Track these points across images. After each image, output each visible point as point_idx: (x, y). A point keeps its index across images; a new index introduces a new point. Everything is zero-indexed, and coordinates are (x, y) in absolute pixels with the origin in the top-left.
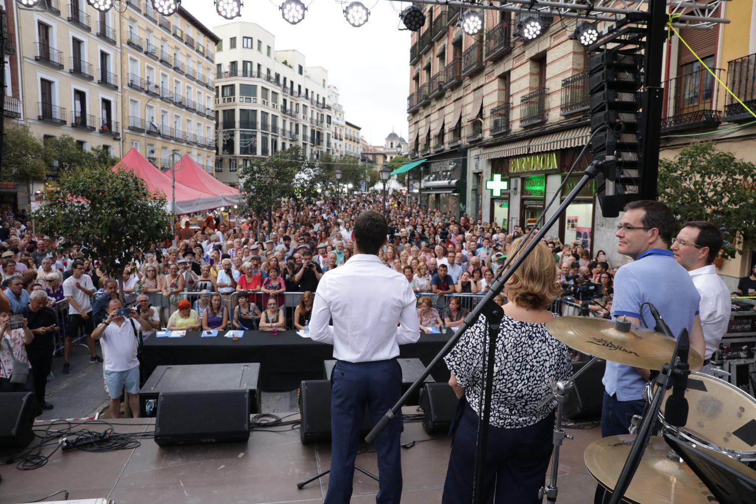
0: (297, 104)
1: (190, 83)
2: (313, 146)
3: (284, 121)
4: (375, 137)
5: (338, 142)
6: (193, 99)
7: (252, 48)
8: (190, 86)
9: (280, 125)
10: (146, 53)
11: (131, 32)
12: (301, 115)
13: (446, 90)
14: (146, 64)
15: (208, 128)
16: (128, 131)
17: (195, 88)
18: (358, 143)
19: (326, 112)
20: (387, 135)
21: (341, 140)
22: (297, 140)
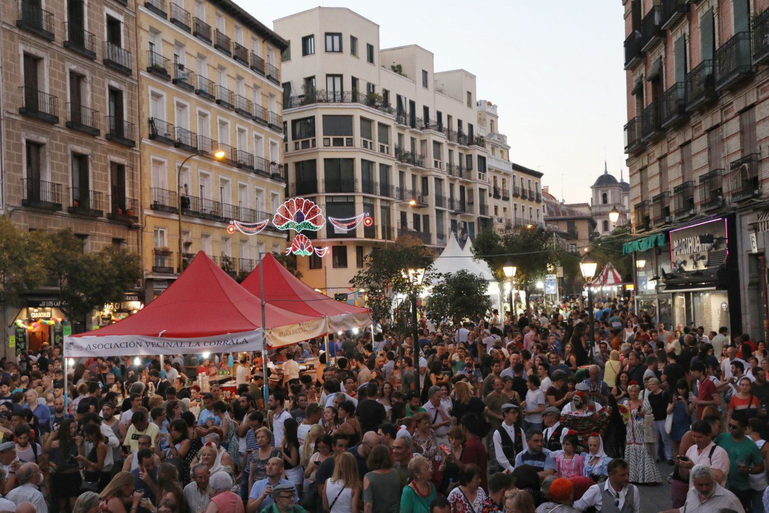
0: (423, 142)
1: (241, 122)
2: (455, 214)
3: (402, 174)
4: (571, 187)
5: (501, 203)
6: (209, 135)
7: (341, 51)
8: (242, 127)
9: (395, 181)
10: (175, 82)
11: (151, 51)
12: (430, 160)
13: (691, 113)
14: (176, 99)
15: (274, 196)
16: (151, 213)
17: (251, 129)
18: (538, 201)
19: (476, 151)
20: (593, 181)
21: (506, 199)
22: (426, 206)
